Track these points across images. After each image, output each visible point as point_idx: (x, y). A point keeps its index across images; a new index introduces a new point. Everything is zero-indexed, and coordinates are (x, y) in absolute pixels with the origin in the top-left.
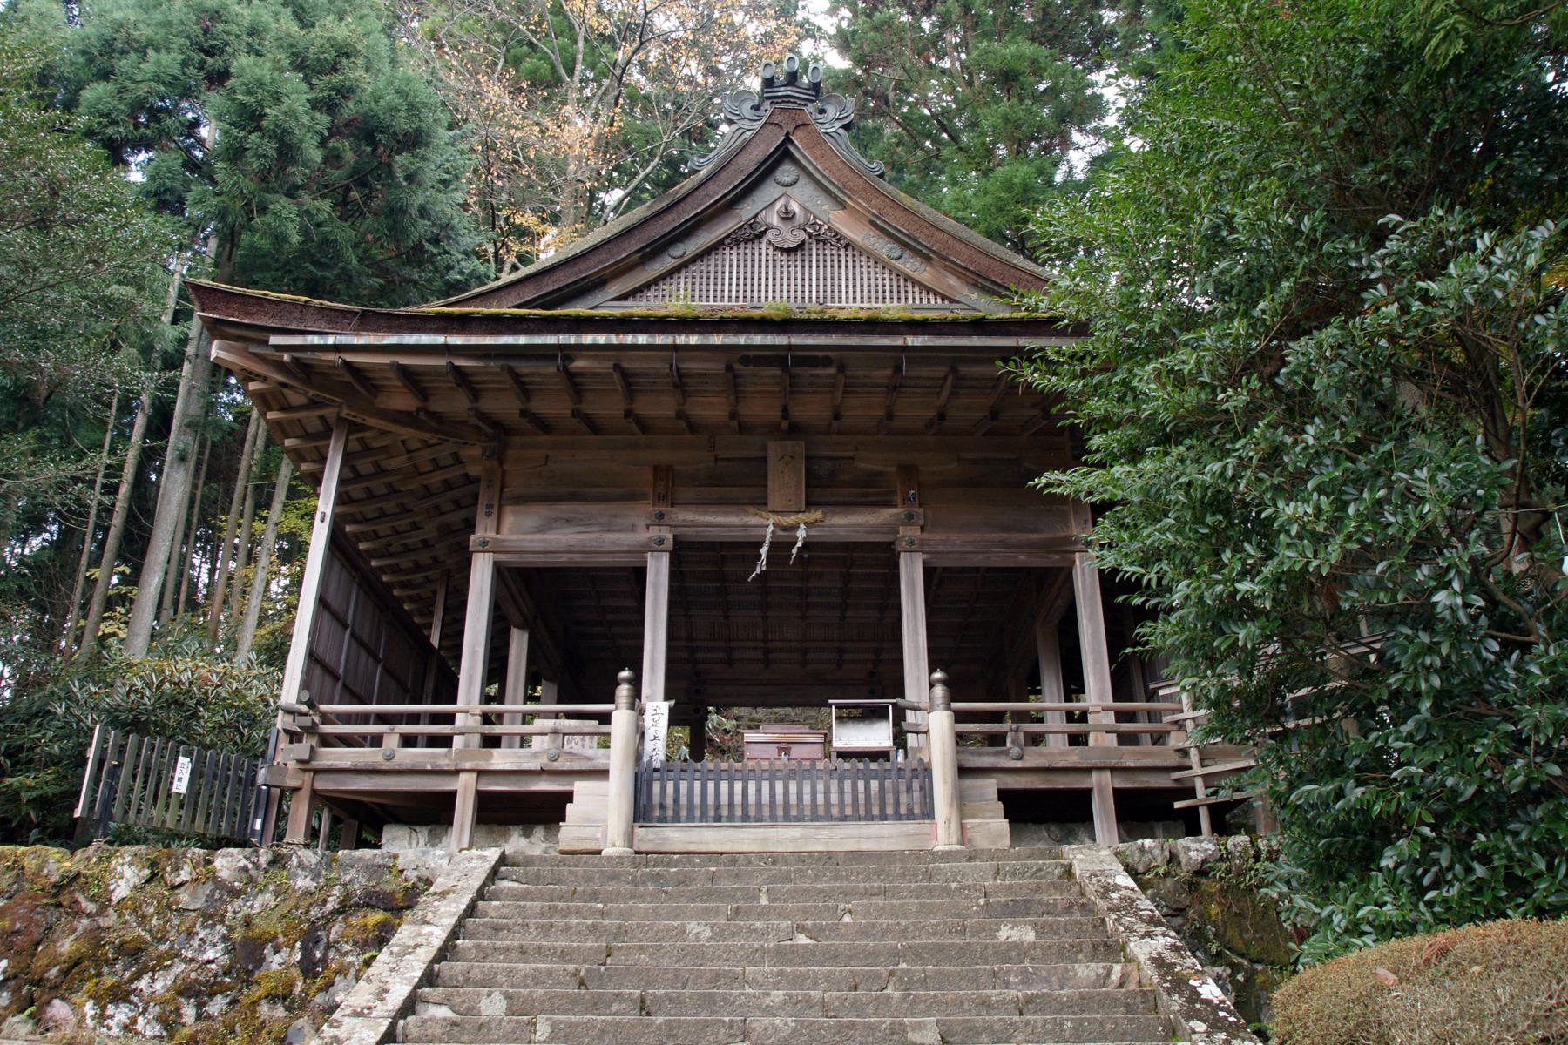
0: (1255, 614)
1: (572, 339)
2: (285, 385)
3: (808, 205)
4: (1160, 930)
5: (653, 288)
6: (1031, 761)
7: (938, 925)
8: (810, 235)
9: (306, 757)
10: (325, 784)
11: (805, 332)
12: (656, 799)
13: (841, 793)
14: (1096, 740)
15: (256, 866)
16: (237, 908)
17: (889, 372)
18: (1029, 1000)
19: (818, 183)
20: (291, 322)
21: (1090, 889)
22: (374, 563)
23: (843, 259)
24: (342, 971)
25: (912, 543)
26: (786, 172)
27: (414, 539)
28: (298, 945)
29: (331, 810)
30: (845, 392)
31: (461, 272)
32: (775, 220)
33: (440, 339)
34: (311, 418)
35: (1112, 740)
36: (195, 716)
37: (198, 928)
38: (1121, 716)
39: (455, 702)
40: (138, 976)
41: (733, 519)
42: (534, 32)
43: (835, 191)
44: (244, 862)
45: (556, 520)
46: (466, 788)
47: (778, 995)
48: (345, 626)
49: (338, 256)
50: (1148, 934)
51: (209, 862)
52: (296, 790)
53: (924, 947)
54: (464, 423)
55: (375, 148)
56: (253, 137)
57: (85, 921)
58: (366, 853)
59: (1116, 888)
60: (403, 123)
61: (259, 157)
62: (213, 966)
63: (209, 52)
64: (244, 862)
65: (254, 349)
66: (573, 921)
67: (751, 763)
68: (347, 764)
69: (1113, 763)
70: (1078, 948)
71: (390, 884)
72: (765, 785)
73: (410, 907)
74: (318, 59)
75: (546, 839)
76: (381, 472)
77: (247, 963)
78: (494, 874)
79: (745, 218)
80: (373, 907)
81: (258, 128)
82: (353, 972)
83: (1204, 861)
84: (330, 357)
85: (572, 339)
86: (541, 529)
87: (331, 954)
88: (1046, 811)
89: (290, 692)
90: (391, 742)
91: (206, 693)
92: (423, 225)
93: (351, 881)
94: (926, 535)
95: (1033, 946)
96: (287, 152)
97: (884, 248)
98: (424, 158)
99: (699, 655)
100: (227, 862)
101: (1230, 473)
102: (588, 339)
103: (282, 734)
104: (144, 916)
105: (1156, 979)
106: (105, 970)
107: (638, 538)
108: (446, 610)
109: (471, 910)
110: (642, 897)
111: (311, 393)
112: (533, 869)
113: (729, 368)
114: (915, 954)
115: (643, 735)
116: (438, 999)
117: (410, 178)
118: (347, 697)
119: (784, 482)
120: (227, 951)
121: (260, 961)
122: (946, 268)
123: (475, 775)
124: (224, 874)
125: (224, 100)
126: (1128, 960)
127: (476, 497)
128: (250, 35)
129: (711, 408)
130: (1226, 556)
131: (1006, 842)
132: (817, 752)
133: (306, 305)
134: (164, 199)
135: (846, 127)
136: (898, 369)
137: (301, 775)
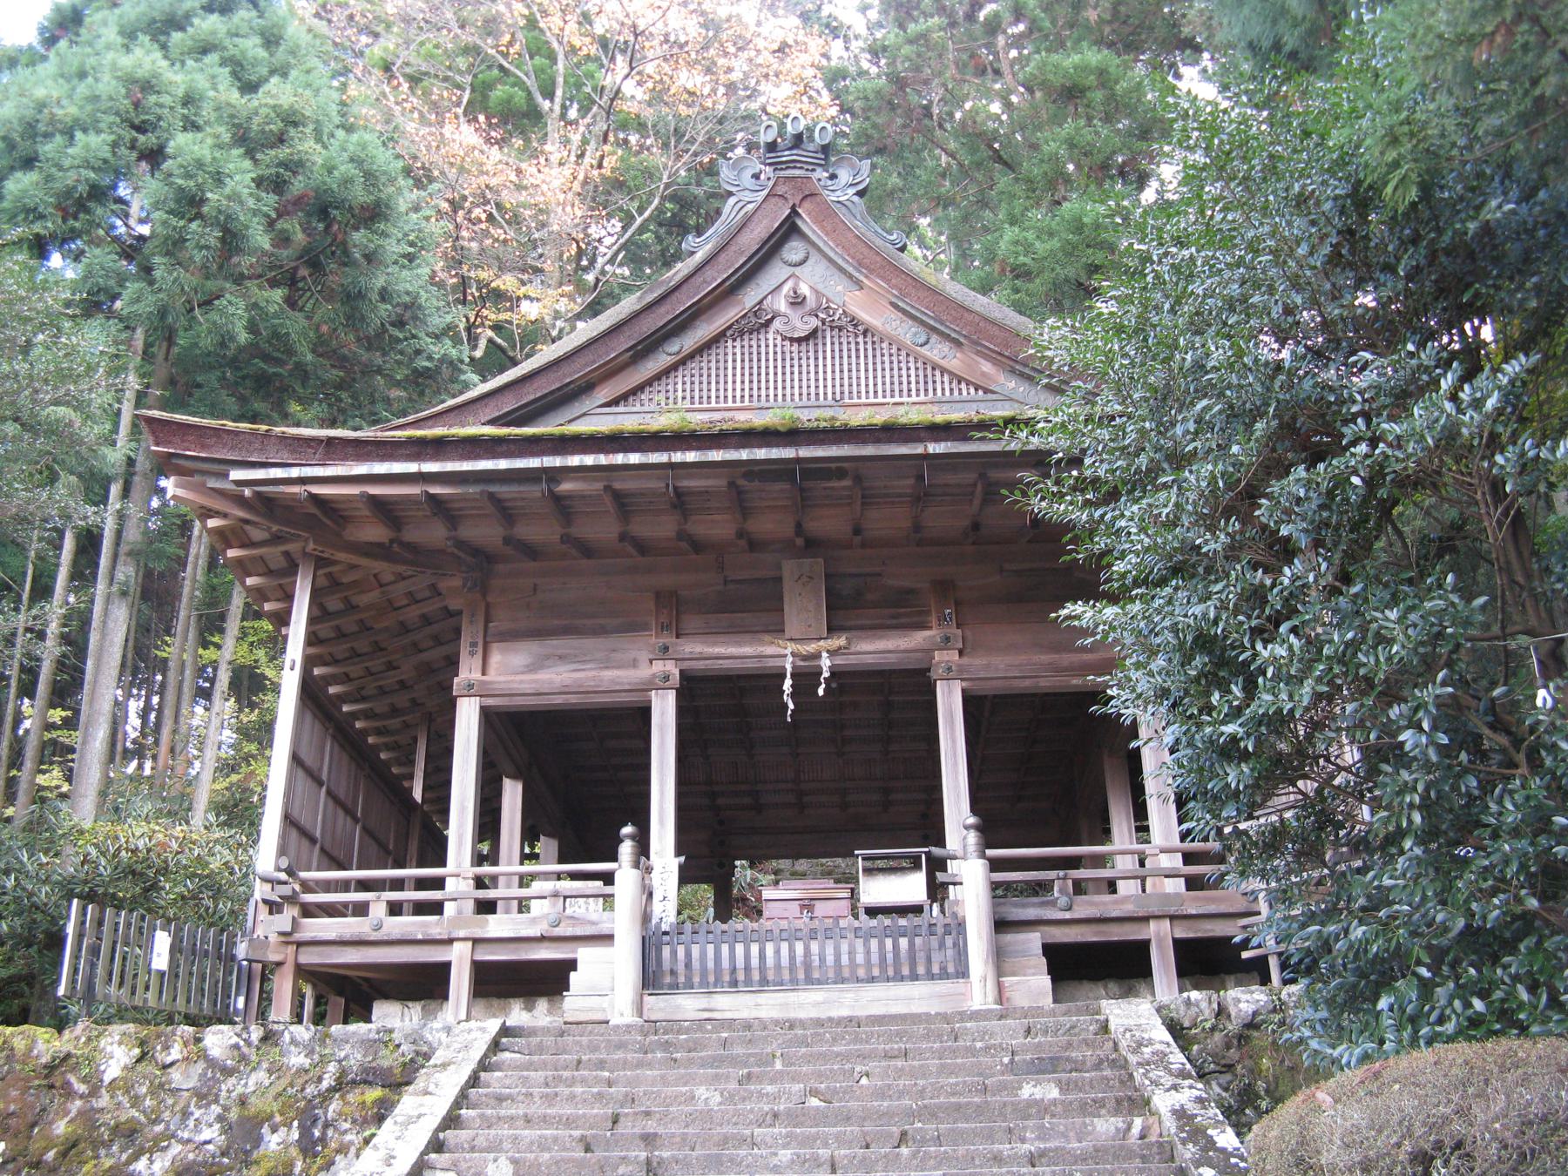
0: (1245, 756)
1: (556, 461)
2: (247, 522)
3: (820, 287)
4: (1187, 1082)
5: (647, 389)
6: (1078, 913)
7: (957, 1084)
9: (289, 929)
10: (309, 957)
11: (814, 444)
12: (666, 965)
13: (868, 952)
14: (1154, 885)
15: (248, 1043)
16: (231, 1087)
17: (911, 481)
18: (1043, 1153)
19: (831, 260)
20: (251, 453)
21: (1123, 1044)
22: (345, 708)
23: (861, 347)
24: (343, 1149)
25: (949, 669)
26: (793, 250)
27: (390, 680)
28: (296, 1123)
29: (314, 986)
30: (863, 504)
31: (430, 358)
32: (782, 305)
33: (412, 467)
34: (273, 554)
35: (1176, 886)
36: (155, 887)
37: (192, 1108)
39: (443, 864)
40: (136, 1157)
41: (747, 650)
42: (505, 55)
44: (235, 1039)
45: (548, 657)
46: (461, 958)
47: (785, 1155)
48: (321, 784)
49: (290, 352)
50: (1175, 1087)
51: (198, 1040)
52: (279, 964)
53: (939, 1106)
54: (442, 551)
55: (329, 229)
56: (194, 226)
57: (78, 1103)
58: (358, 1028)
59: (1150, 1042)
60: (359, 195)
61: (202, 248)
62: (210, 1147)
63: (141, 129)
64: (235, 1039)
65: (213, 483)
66: (579, 1090)
67: (769, 923)
68: (332, 936)
69: (1172, 910)
70: (1100, 1103)
71: (387, 1060)
73: (408, 1083)
74: (263, 132)
75: (550, 1012)
76: (351, 608)
77: (245, 1142)
78: (495, 1046)
80: (370, 1083)
81: (198, 216)
82: (353, 1150)
83: (1255, 1014)
84: (295, 489)
85: (556, 461)
86: (532, 668)
87: (330, 1132)
89: (266, 857)
90: (378, 910)
91: (166, 861)
92: (384, 309)
93: (346, 1057)
94: (965, 660)
95: (1054, 1102)
96: (231, 240)
97: (907, 332)
98: (384, 234)
99: (721, 801)
100: (218, 1040)
101: (1212, 616)
102: (575, 460)
103: (261, 905)
104: (137, 1097)
105: (1173, 1131)
106: (102, 1152)
107: (642, 672)
108: (429, 757)
109: (474, 1081)
110: (650, 1065)
111: (275, 528)
112: (534, 1040)
113: (732, 484)
114: (931, 1114)
115: (650, 895)
116: (445, 1166)
117: (370, 258)
118: (326, 860)
120: (223, 1132)
121: (258, 1141)
122: (978, 353)
123: (470, 944)
124: (215, 1052)
125: (161, 184)
126: (1152, 1114)
127: (458, 632)
128: (185, 104)
129: (717, 526)
130: (1215, 698)
131: (1047, 1001)
132: (844, 907)
133: (267, 434)
134: (95, 303)
135: (861, 194)
136: (921, 478)
137: (283, 948)
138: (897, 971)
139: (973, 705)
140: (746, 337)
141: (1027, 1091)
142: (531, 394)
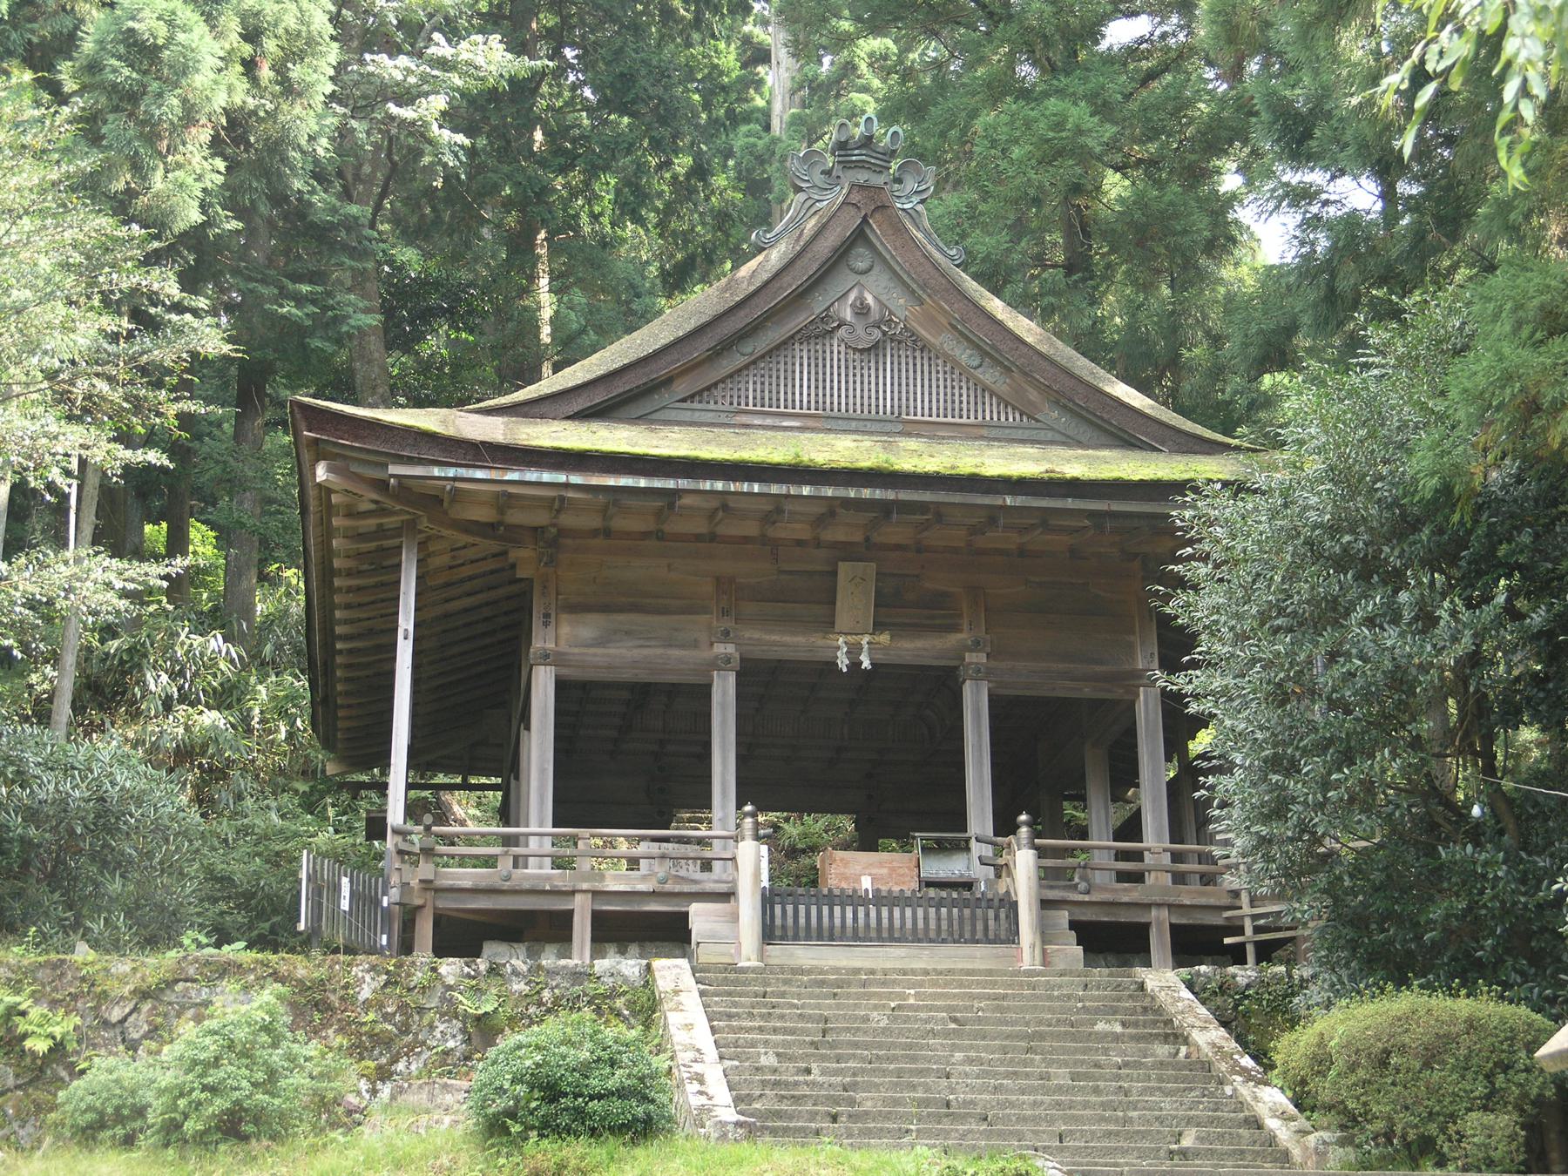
1: (683, 483)
3: (883, 298)
5: (721, 386)
8: (884, 333)
10: (446, 903)
25: (979, 671)
32: (848, 315)
33: (561, 478)
38: (1177, 857)
40: (395, 1061)
41: (800, 640)
43: (914, 286)
52: (421, 907)
68: (467, 884)
69: (1171, 900)
72: (849, 910)
79: (817, 312)
86: (600, 642)
88: (1112, 941)
90: (505, 865)
94: (993, 664)
97: (965, 356)
119: (854, 596)
138: (961, 936)
139: (1003, 711)
140: (812, 341)
141: (1100, 1026)
142: (621, 387)
